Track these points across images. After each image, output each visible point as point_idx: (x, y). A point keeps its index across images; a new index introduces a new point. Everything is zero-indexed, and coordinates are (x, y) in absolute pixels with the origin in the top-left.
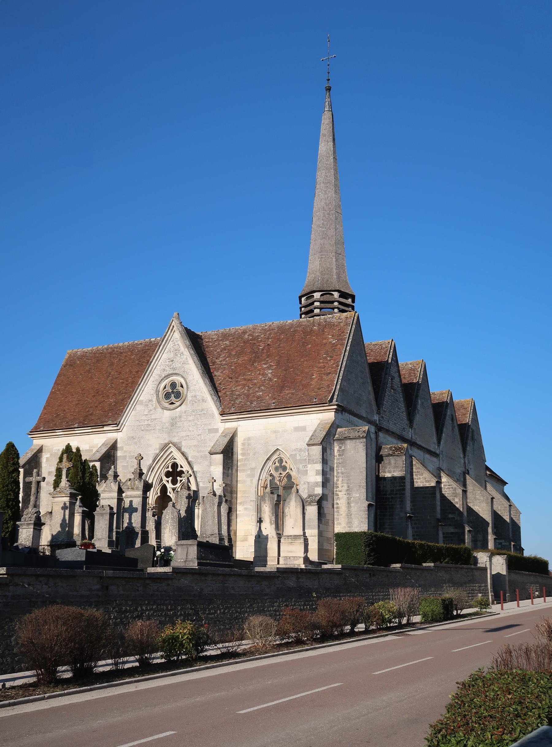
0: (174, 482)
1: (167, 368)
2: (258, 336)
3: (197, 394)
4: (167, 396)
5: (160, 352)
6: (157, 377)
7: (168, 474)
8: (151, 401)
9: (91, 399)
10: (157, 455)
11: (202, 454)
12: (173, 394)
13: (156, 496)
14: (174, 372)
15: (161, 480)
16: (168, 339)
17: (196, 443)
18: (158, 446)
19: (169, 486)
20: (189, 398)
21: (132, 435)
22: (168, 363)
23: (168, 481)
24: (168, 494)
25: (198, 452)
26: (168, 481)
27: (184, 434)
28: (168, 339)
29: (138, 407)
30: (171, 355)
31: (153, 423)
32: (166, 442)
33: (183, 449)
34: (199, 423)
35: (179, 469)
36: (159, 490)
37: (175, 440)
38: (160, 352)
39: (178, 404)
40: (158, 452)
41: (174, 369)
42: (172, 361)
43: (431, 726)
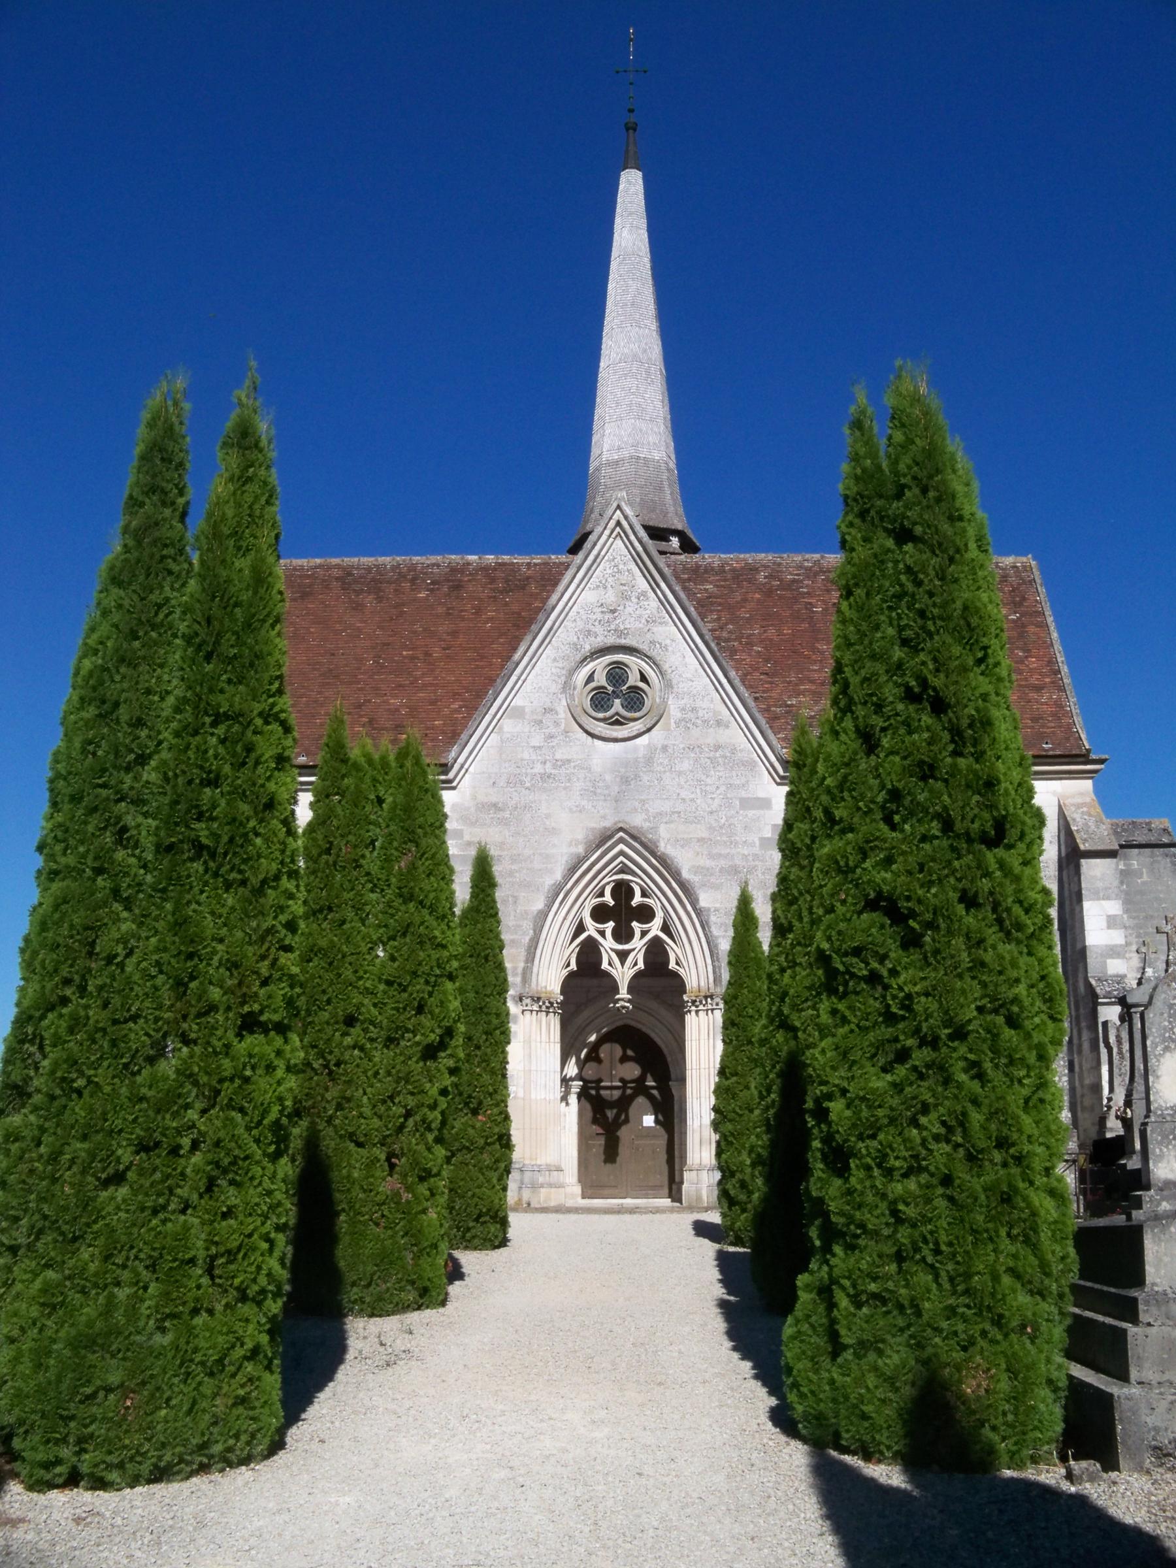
0: (623, 934)
1: (599, 629)
2: (794, 581)
3: (699, 703)
4: (600, 700)
5: (578, 586)
6: (566, 650)
7: (600, 914)
8: (548, 710)
9: (320, 693)
10: (580, 861)
11: (723, 863)
12: (619, 696)
13: (565, 972)
14: (623, 642)
15: (581, 928)
16: (599, 554)
17: (704, 834)
18: (580, 835)
19: (608, 944)
20: (674, 710)
21: (494, 799)
22: (599, 616)
23: (602, 933)
24: (605, 965)
25: (711, 856)
26: (602, 933)
27: (666, 807)
28: (599, 554)
29: (508, 725)
30: (610, 597)
31: (563, 771)
32: (608, 823)
33: (664, 847)
34: (709, 781)
35: (608, 899)
36: (574, 956)
37: (637, 821)
38: (578, 586)
39: (637, 727)
40: (581, 850)
41: (620, 633)
42: (613, 611)
43: (822, 1535)
